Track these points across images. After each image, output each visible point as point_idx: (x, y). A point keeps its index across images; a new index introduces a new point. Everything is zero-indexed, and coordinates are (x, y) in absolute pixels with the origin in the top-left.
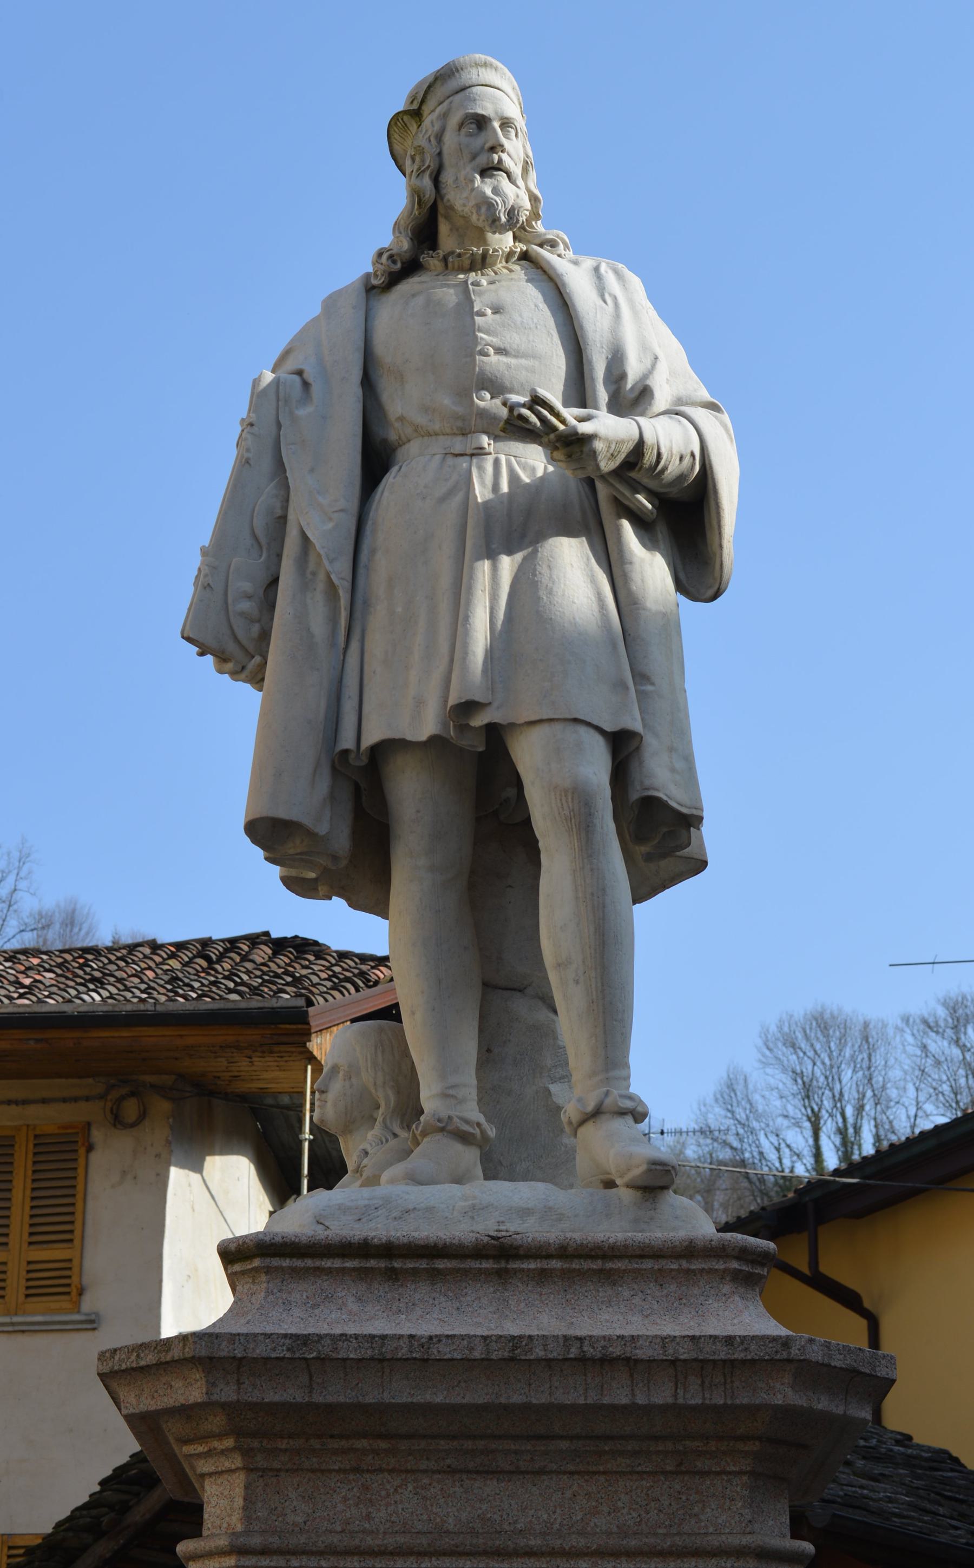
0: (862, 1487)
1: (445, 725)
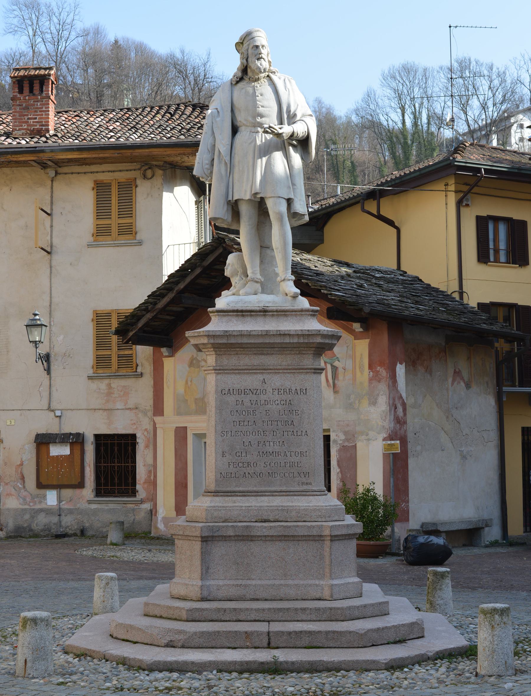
0: (384, 296)
1: (251, 197)
